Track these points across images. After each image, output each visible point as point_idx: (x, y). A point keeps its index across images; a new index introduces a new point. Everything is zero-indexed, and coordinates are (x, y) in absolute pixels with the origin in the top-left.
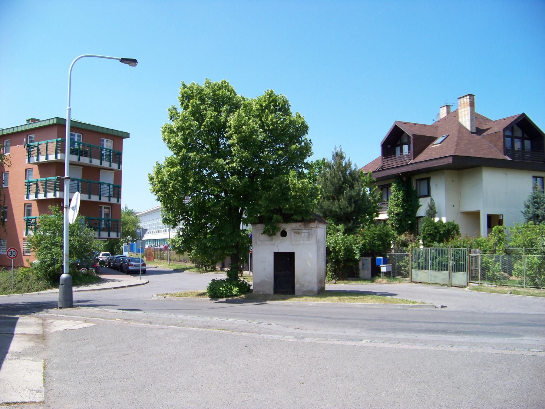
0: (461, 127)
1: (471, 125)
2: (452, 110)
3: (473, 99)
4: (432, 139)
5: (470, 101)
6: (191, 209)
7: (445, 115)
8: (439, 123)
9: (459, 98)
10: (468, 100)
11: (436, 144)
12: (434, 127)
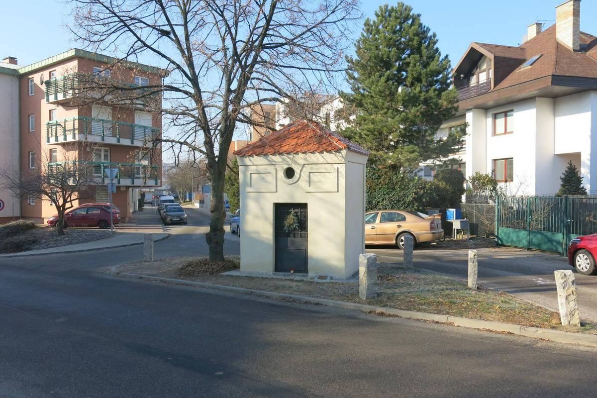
0: (559, 47)
1: (574, 41)
2: (544, 29)
3: (579, 6)
4: (519, 62)
5: (574, 9)
6: (254, 50)
7: (535, 35)
8: (527, 44)
9: (348, 161)
10: (572, 8)
11: (525, 67)
12: (522, 49)
